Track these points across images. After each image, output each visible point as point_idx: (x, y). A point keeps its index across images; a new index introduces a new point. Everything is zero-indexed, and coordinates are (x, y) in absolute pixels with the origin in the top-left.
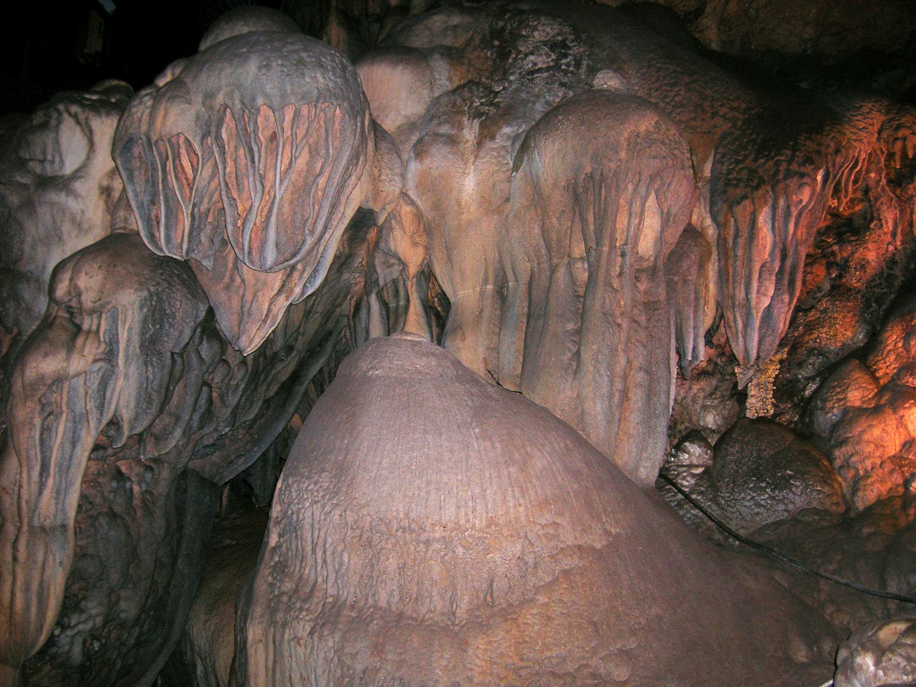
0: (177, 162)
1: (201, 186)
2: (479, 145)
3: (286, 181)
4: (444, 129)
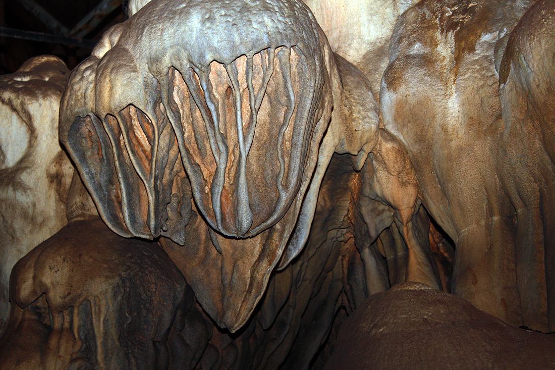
0: (131, 135)
1: (161, 155)
2: (458, 59)
3: (251, 135)
4: (417, 48)
